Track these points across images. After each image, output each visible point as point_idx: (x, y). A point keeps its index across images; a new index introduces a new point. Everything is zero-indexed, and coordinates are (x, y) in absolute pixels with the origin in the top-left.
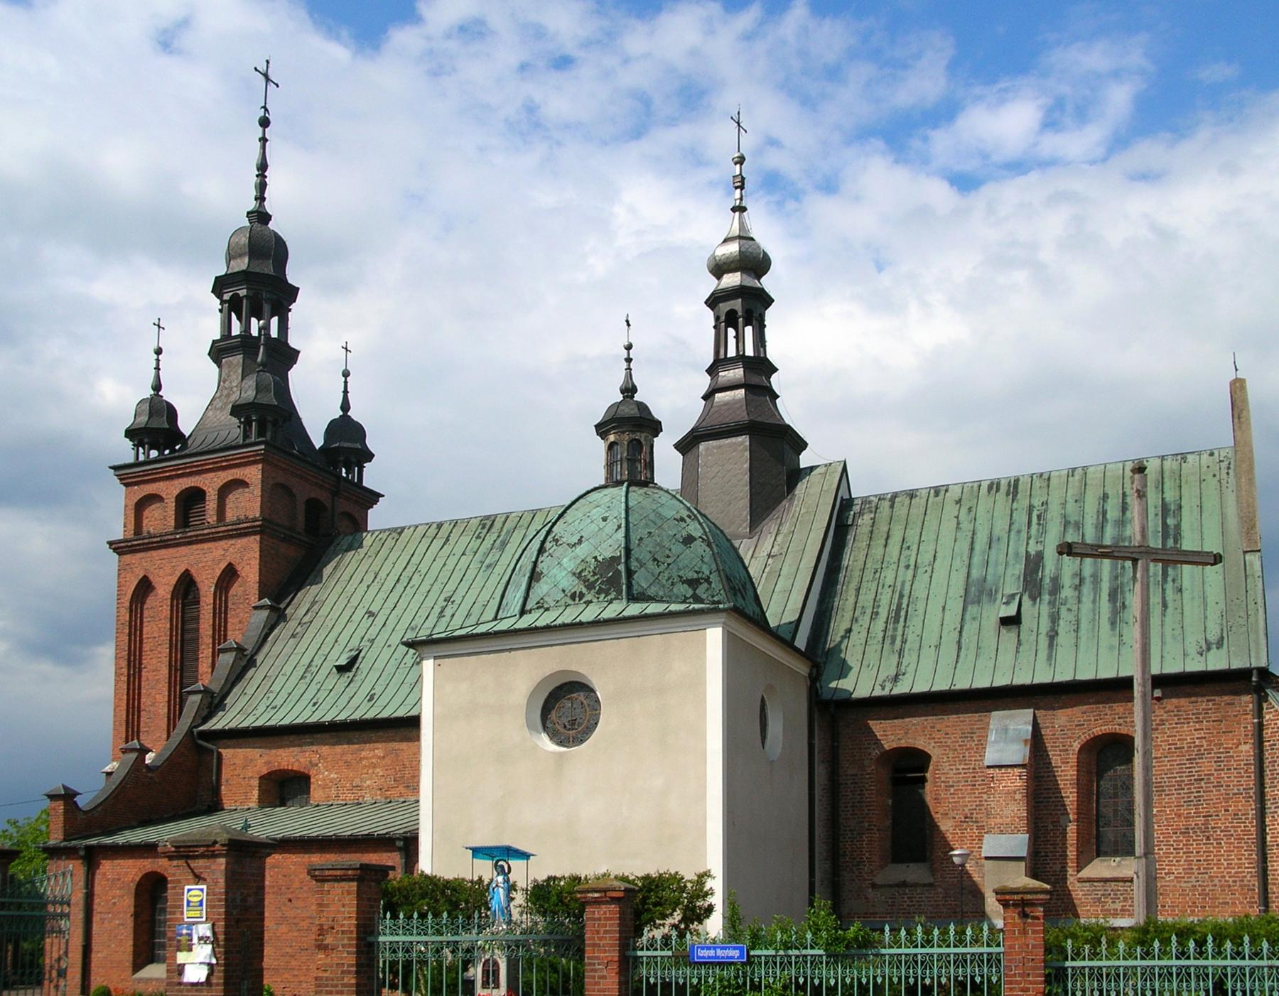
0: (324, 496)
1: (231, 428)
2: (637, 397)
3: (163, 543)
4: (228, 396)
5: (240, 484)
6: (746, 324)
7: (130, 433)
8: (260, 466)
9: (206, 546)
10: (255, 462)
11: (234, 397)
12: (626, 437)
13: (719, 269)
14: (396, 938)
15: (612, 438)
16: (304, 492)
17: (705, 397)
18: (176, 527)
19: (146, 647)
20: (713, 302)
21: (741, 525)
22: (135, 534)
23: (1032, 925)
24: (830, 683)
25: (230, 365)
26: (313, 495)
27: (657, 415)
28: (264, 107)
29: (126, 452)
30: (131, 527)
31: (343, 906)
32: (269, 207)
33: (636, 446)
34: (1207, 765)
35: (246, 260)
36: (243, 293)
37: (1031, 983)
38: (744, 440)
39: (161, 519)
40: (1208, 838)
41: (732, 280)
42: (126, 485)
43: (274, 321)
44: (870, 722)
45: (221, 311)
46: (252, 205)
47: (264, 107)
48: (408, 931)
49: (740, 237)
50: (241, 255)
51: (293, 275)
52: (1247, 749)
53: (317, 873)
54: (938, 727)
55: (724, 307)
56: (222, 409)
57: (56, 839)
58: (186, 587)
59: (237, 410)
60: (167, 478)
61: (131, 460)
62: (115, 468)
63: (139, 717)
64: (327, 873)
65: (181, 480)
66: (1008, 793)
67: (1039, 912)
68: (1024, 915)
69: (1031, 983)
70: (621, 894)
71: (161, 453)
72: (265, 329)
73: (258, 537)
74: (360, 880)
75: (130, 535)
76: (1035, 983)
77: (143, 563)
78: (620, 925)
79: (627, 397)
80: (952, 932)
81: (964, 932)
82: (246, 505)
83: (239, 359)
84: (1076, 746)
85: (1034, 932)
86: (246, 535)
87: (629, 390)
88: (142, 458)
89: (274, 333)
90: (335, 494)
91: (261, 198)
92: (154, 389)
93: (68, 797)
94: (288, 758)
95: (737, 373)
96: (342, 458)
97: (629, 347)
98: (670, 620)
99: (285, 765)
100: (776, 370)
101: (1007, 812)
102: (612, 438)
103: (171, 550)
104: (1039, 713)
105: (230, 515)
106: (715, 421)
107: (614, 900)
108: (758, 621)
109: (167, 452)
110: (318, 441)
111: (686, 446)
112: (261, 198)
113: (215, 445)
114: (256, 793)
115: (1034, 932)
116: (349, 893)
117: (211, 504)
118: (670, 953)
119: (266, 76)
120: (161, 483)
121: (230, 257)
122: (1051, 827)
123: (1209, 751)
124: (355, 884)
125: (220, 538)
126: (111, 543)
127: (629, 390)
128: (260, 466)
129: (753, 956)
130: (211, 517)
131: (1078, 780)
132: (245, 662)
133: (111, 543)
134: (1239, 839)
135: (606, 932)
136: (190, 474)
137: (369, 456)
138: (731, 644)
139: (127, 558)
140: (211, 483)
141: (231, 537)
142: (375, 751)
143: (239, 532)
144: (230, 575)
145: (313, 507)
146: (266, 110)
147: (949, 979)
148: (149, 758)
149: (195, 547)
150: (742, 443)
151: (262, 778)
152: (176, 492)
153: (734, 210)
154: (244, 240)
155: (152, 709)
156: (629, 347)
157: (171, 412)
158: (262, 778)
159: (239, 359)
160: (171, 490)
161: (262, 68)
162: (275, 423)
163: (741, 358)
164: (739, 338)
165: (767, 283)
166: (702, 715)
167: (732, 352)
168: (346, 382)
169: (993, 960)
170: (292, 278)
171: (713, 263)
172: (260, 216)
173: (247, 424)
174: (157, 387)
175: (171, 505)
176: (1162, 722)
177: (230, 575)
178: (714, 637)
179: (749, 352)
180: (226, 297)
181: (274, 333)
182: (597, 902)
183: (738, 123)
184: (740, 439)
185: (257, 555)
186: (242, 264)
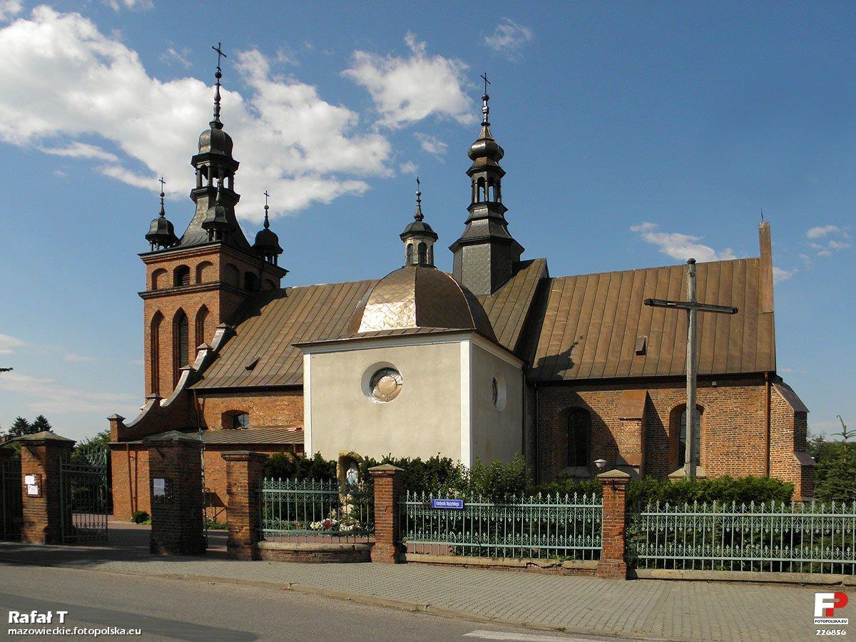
0: (255, 271)
1: (203, 234)
2: (423, 221)
3: (168, 294)
4: (201, 218)
5: (208, 263)
6: (489, 186)
7: (149, 237)
8: (219, 255)
9: (190, 295)
10: (216, 253)
11: (204, 219)
12: (419, 242)
13: (475, 155)
14: (270, 491)
15: (409, 242)
16: (244, 268)
17: (467, 223)
18: (174, 286)
19: (161, 347)
20: (470, 173)
21: (486, 290)
22: (153, 289)
23: (618, 494)
24: (559, 371)
25: (202, 202)
26: (249, 270)
27: (435, 231)
28: (218, 68)
29: (147, 247)
30: (150, 285)
31: (241, 473)
32: (221, 120)
33: (422, 248)
34: (739, 420)
35: (210, 147)
36: (208, 164)
37: (617, 523)
38: (488, 246)
39: (166, 281)
40: (739, 458)
41: (482, 161)
42: (147, 264)
43: (226, 180)
44: (580, 394)
45: (196, 174)
46: (213, 119)
47: (218, 68)
48: (276, 487)
49: (485, 139)
50: (207, 145)
51: (236, 155)
52: (762, 413)
53: (227, 456)
54: (594, 397)
55: (477, 176)
56: (197, 225)
57: (114, 440)
58: (181, 317)
59: (205, 225)
60: (169, 260)
61: (150, 251)
62: (141, 255)
63: (158, 382)
64: (232, 456)
65: (176, 261)
66: (631, 432)
67: (623, 487)
68: (615, 489)
69: (617, 523)
70: (394, 473)
71: (166, 247)
72: (221, 183)
73: (218, 291)
74: (249, 461)
75: (150, 289)
76: (620, 523)
77: (156, 304)
78: (393, 488)
79: (418, 220)
80: (576, 497)
81: (582, 497)
82: (212, 274)
83: (206, 199)
84: (670, 409)
85: (619, 497)
86: (212, 290)
87: (420, 217)
88: (155, 250)
89: (226, 185)
90: (261, 270)
91: (217, 115)
92: (161, 214)
93: (119, 420)
94: (236, 403)
95: (484, 211)
96: (265, 251)
97: (419, 194)
98: (427, 338)
99: (235, 408)
100: (506, 210)
101: (630, 442)
102: (409, 242)
103: (173, 297)
104: (650, 391)
105: (204, 280)
106: (470, 236)
107: (390, 476)
108: (492, 339)
109: (169, 247)
110: (251, 241)
111: (457, 247)
112: (217, 115)
113: (195, 243)
114: (220, 421)
115: (619, 497)
116: (244, 467)
117: (193, 274)
118: (421, 503)
119: (219, 51)
120: (166, 263)
121: (200, 146)
122: (654, 450)
123: (741, 414)
124: (247, 462)
125: (198, 292)
126: (139, 294)
127: (420, 217)
128: (219, 255)
129: (467, 506)
130: (193, 282)
131: (670, 427)
132: (212, 357)
133: (139, 294)
134: (755, 458)
135: (385, 491)
136: (181, 258)
137: (281, 251)
138: (474, 350)
139: (149, 301)
140: (192, 263)
141: (204, 291)
142: (284, 400)
143: (209, 289)
144: (204, 311)
145: (249, 276)
146: (219, 69)
147: (573, 520)
148: (162, 403)
149: (184, 296)
150: (486, 248)
151: (223, 414)
152: (174, 267)
153: (483, 124)
154: (208, 137)
155: (165, 378)
156: (419, 194)
157: (171, 227)
158: (223, 414)
159: (206, 199)
160: (171, 266)
161: (217, 46)
162: (226, 232)
163: (487, 203)
164: (486, 192)
165: (502, 164)
166: (458, 386)
167: (482, 200)
168: (267, 212)
169: (598, 511)
170: (235, 158)
171: (471, 153)
172: (217, 125)
173: (211, 232)
174: (163, 213)
175: (171, 274)
176: (716, 399)
177: (204, 311)
178: (465, 346)
179: (492, 200)
180: (199, 167)
181: (226, 185)
182: (380, 476)
183: (485, 79)
184: (485, 245)
185: (218, 300)
186: (207, 149)
